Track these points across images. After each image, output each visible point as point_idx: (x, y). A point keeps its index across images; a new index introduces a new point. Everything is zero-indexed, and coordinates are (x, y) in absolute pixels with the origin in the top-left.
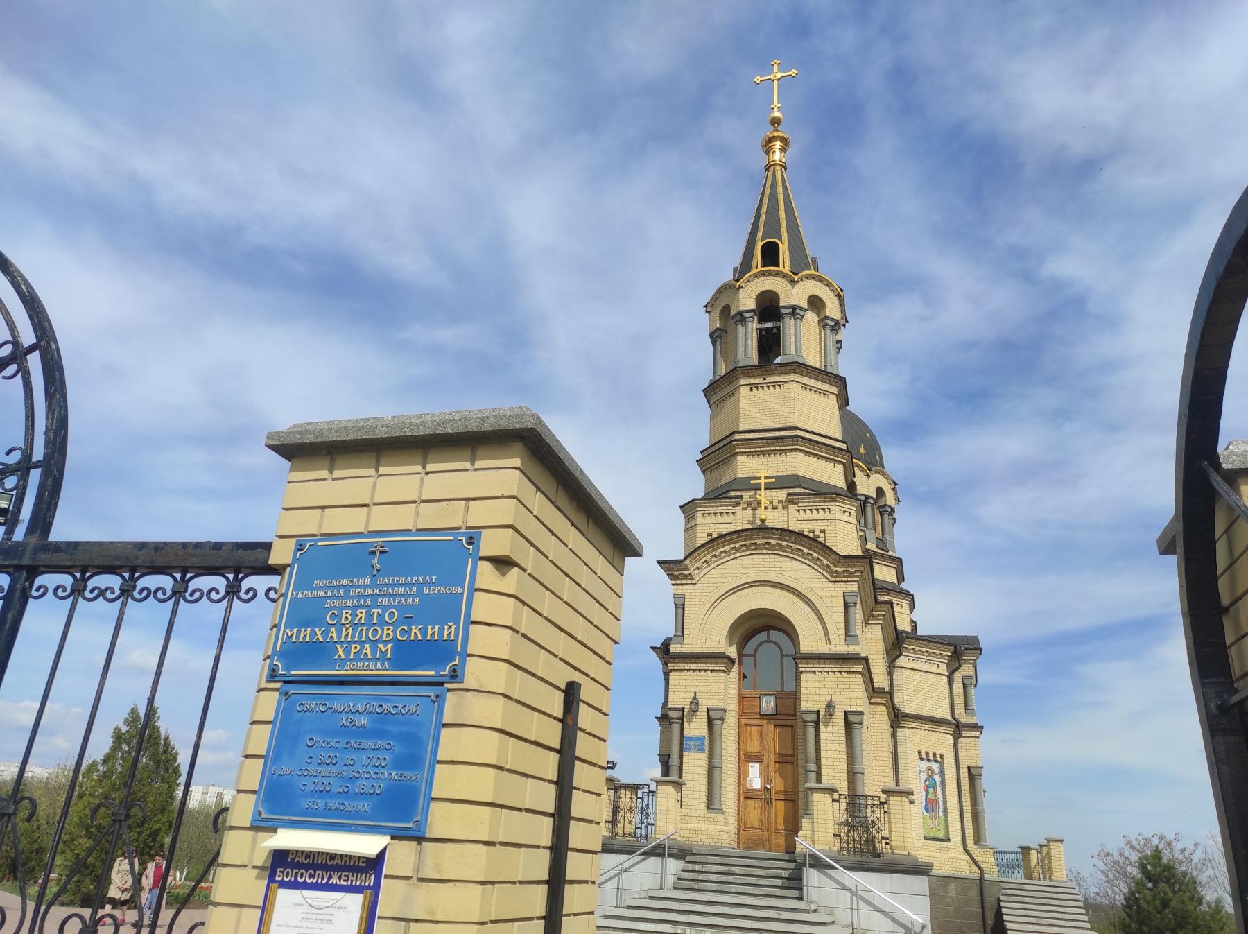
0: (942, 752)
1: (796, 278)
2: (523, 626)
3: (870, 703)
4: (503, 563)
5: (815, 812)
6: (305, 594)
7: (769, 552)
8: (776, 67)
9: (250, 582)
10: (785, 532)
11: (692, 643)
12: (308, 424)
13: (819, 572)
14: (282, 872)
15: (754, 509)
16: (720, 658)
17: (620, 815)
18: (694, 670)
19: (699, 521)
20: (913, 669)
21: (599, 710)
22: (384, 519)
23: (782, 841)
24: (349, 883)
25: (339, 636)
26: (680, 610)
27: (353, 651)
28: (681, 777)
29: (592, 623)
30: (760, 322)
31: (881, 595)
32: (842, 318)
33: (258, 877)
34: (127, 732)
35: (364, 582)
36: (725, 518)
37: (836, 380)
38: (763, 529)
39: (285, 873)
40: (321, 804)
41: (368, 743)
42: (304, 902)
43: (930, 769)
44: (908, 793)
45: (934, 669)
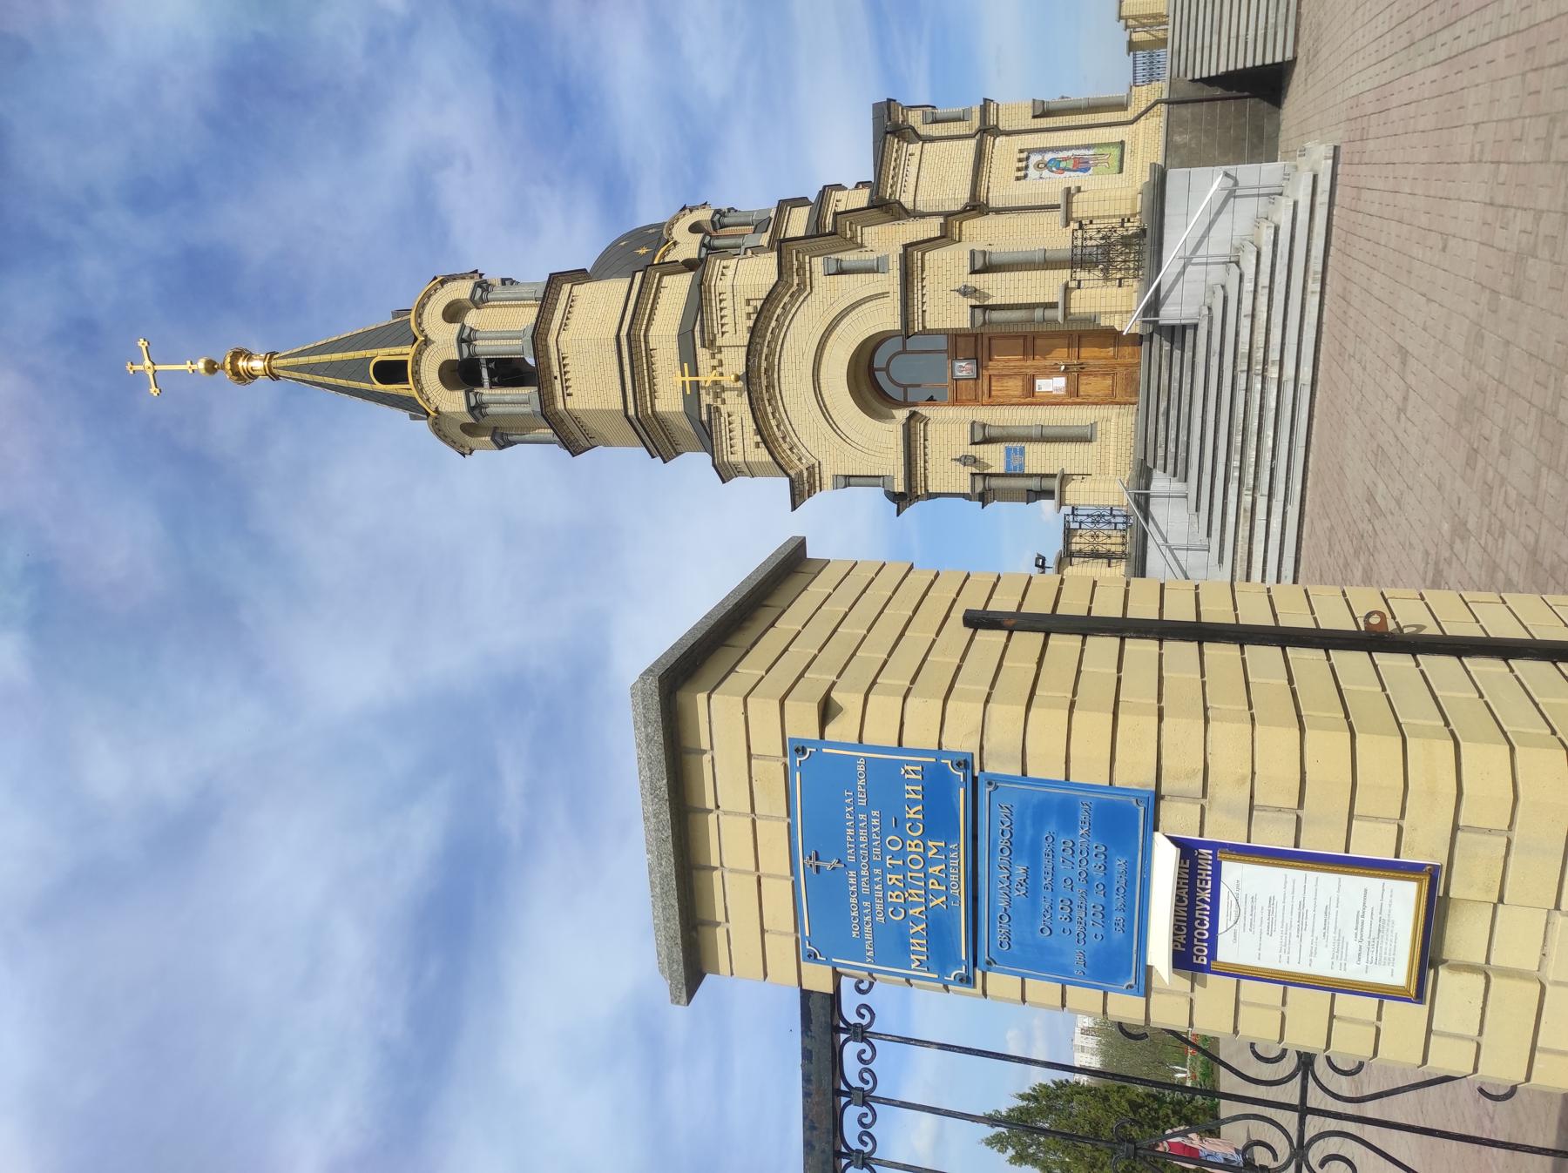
0: (1016, 150)
1: (421, 338)
2: (901, 683)
3: (960, 241)
4: (827, 711)
5: (1093, 310)
6: (869, 948)
7: (776, 370)
8: (137, 367)
9: (850, 1014)
10: (751, 351)
11: (892, 465)
12: (659, 955)
13: (800, 306)
14: (1198, 957)
15: (723, 389)
16: (909, 430)
17: (1100, 549)
18: (925, 462)
19: (741, 459)
20: (916, 186)
21: (995, 585)
22: (776, 857)
23: (1127, 350)
24: (1209, 878)
25: (919, 904)
26: (852, 480)
27: (937, 887)
28: (1054, 476)
29: (890, 598)
30: (481, 385)
31: (825, 228)
32: (472, 278)
33: (1204, 986)
34: (1014, 1148)
35: (853, 877)
36: (736, 426)
37: (554, 286)
38: (748, 378)
39: (1200, 954)
40: (1118, 916)
41: (1046, 864)
42: (1232, 931)
43: (1037, 166)
44: (1068, 194)
45: (915, 160)
